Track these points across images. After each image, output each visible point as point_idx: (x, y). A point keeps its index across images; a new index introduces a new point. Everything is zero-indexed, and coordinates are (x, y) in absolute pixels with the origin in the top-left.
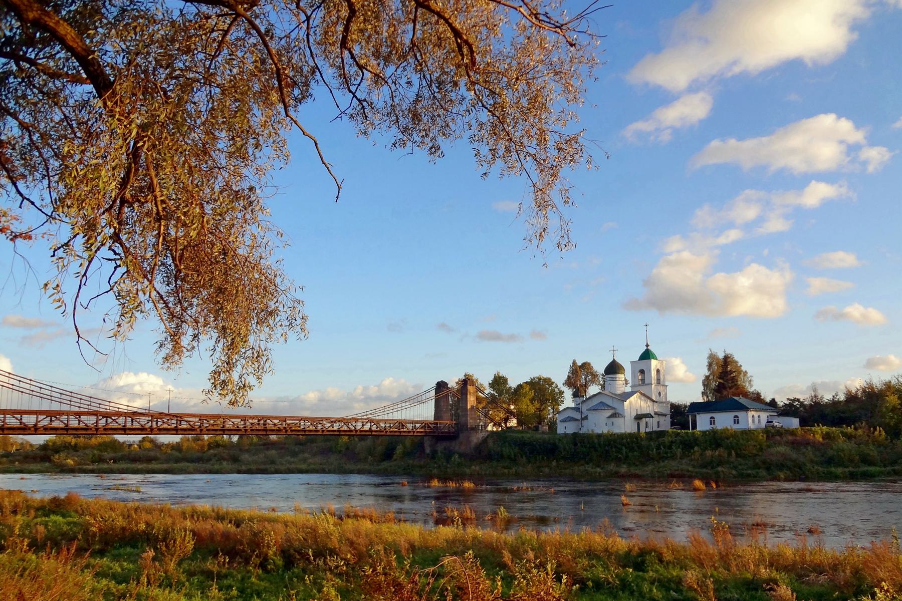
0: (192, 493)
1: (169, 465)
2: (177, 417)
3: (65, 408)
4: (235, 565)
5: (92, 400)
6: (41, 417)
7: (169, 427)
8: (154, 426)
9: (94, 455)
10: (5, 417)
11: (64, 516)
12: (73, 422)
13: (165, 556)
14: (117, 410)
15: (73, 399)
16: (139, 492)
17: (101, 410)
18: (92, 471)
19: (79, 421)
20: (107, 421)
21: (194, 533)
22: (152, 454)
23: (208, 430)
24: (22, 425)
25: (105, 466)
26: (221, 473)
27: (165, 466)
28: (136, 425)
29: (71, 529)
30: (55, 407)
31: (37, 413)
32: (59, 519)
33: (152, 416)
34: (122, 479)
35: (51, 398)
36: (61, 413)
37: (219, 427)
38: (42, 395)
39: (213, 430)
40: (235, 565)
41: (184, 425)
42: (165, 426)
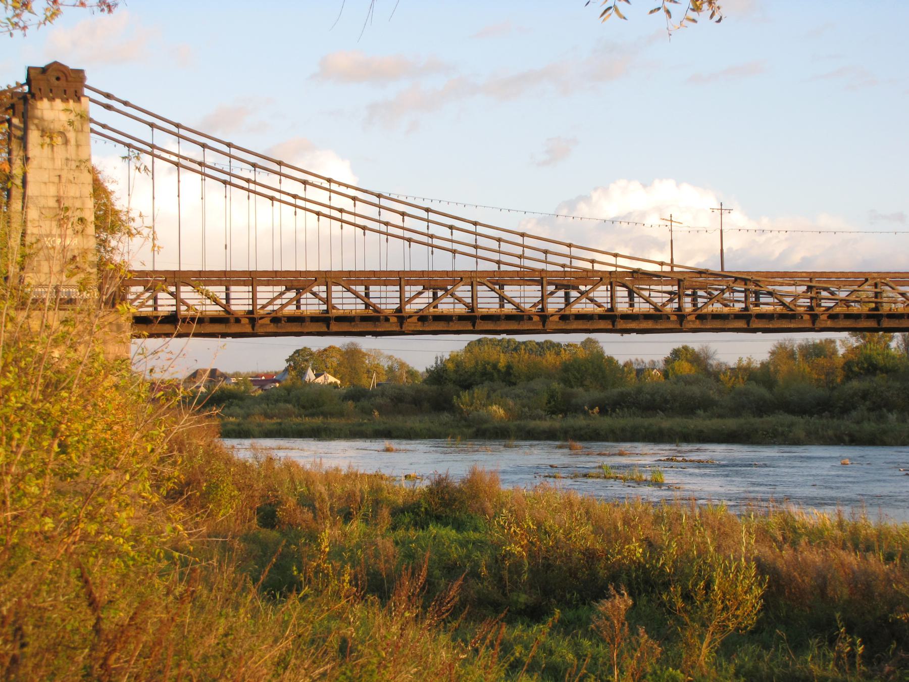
0: (799, 492)
1: (742, 421)
2: (745, 281)
3: (465, 264)
4: (887, 669)
5: (528, 241)
6: (410, 290)
7: (726, 310)
8: (688, 306)
9: (552, 396)
10: (328, 292)
11: (459, 526)
12: (487, 301)
13: (684, 625)
14: (588, 266)
15: (482, 242)
16: (658, 484)
17: (550, 268)
18: (549, 435)
19: (502, 298)
20: (567, 296)
21: (762, 568)
22: (696, 390)
23: (833, 317)
24: (370, 312)
25: (580, 421)
26: (884, 444)
27: (731, 423)
28: (641, 306)
29: (468, 557)
30: (442, 262)
31: (400, 279)
32: (449, 533)
33: (679, 282)
34: (621, 454)
35: (431, 243)
36: (458, 278)
37: (865, 309)
38: (408, 235)
39: (848, 316)
40: (887, 669)
41: (768, 305)
42: (717, 307)
